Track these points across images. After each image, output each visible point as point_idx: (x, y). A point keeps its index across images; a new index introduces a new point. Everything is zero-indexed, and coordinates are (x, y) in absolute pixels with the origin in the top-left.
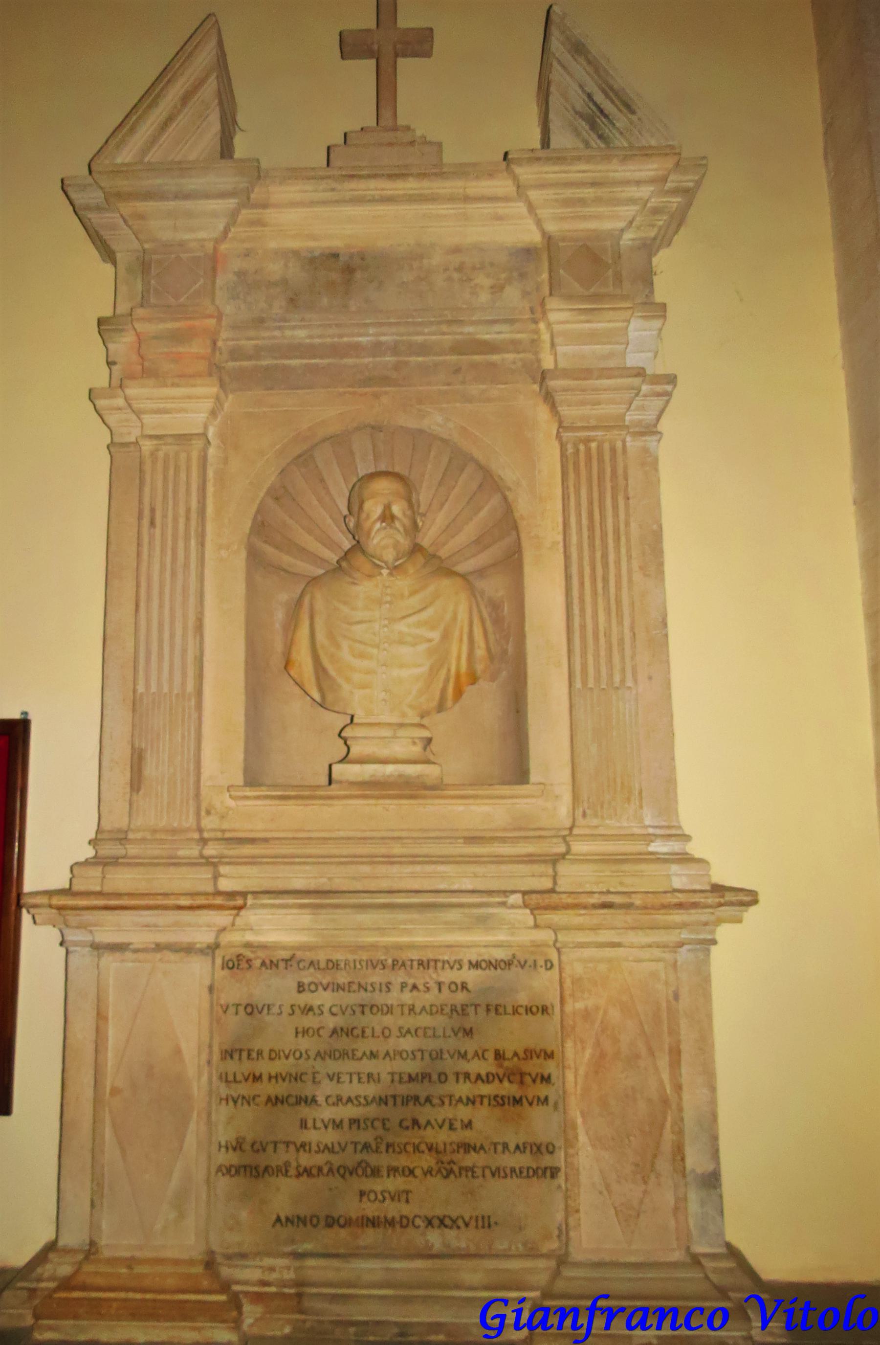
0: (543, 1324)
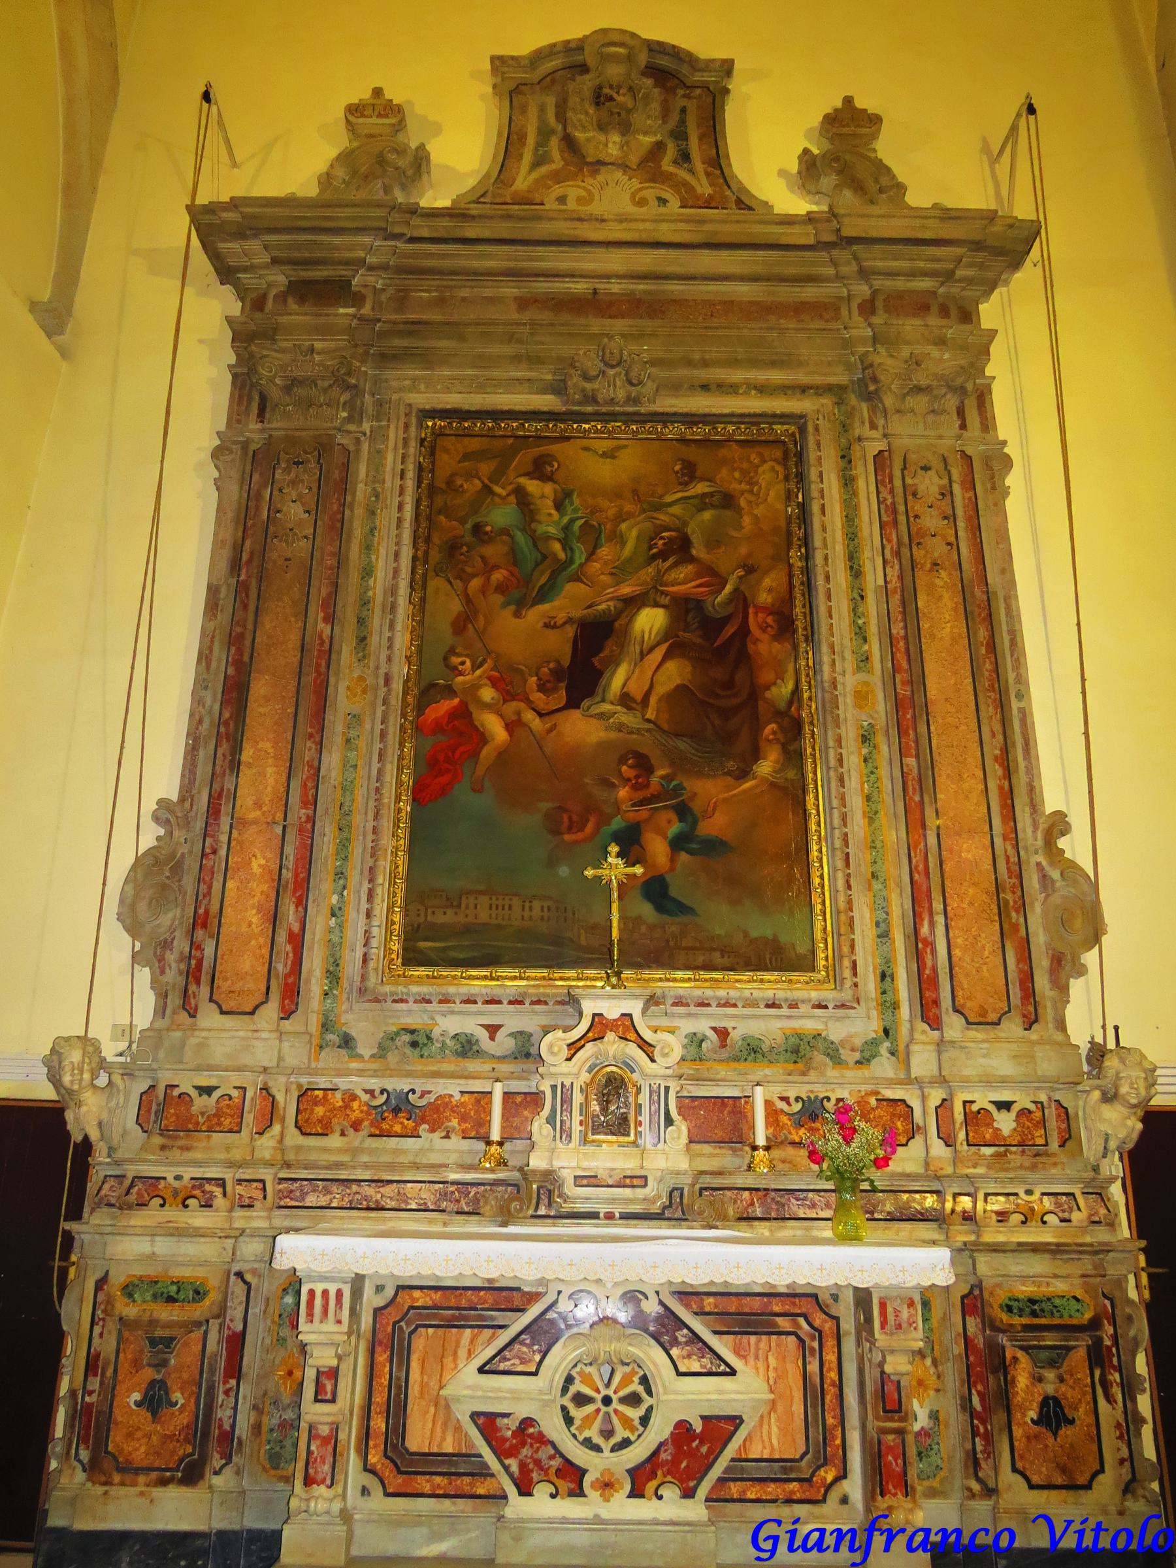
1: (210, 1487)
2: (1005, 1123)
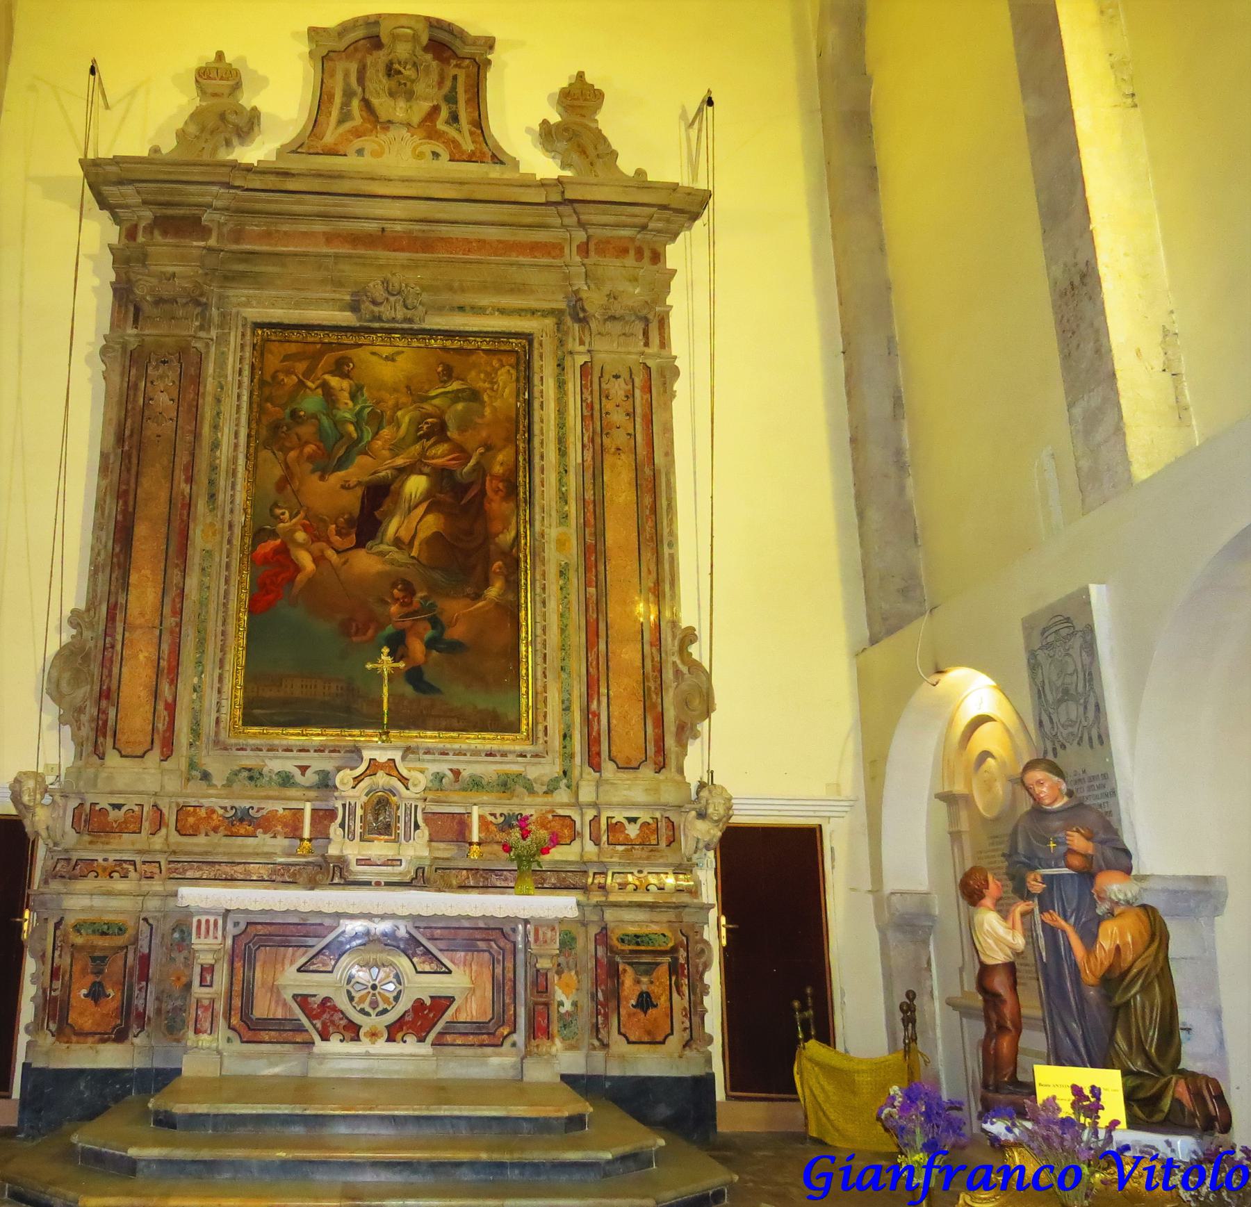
0: (875, 1183)
1: (132, 1044)
2: (633, 831)
